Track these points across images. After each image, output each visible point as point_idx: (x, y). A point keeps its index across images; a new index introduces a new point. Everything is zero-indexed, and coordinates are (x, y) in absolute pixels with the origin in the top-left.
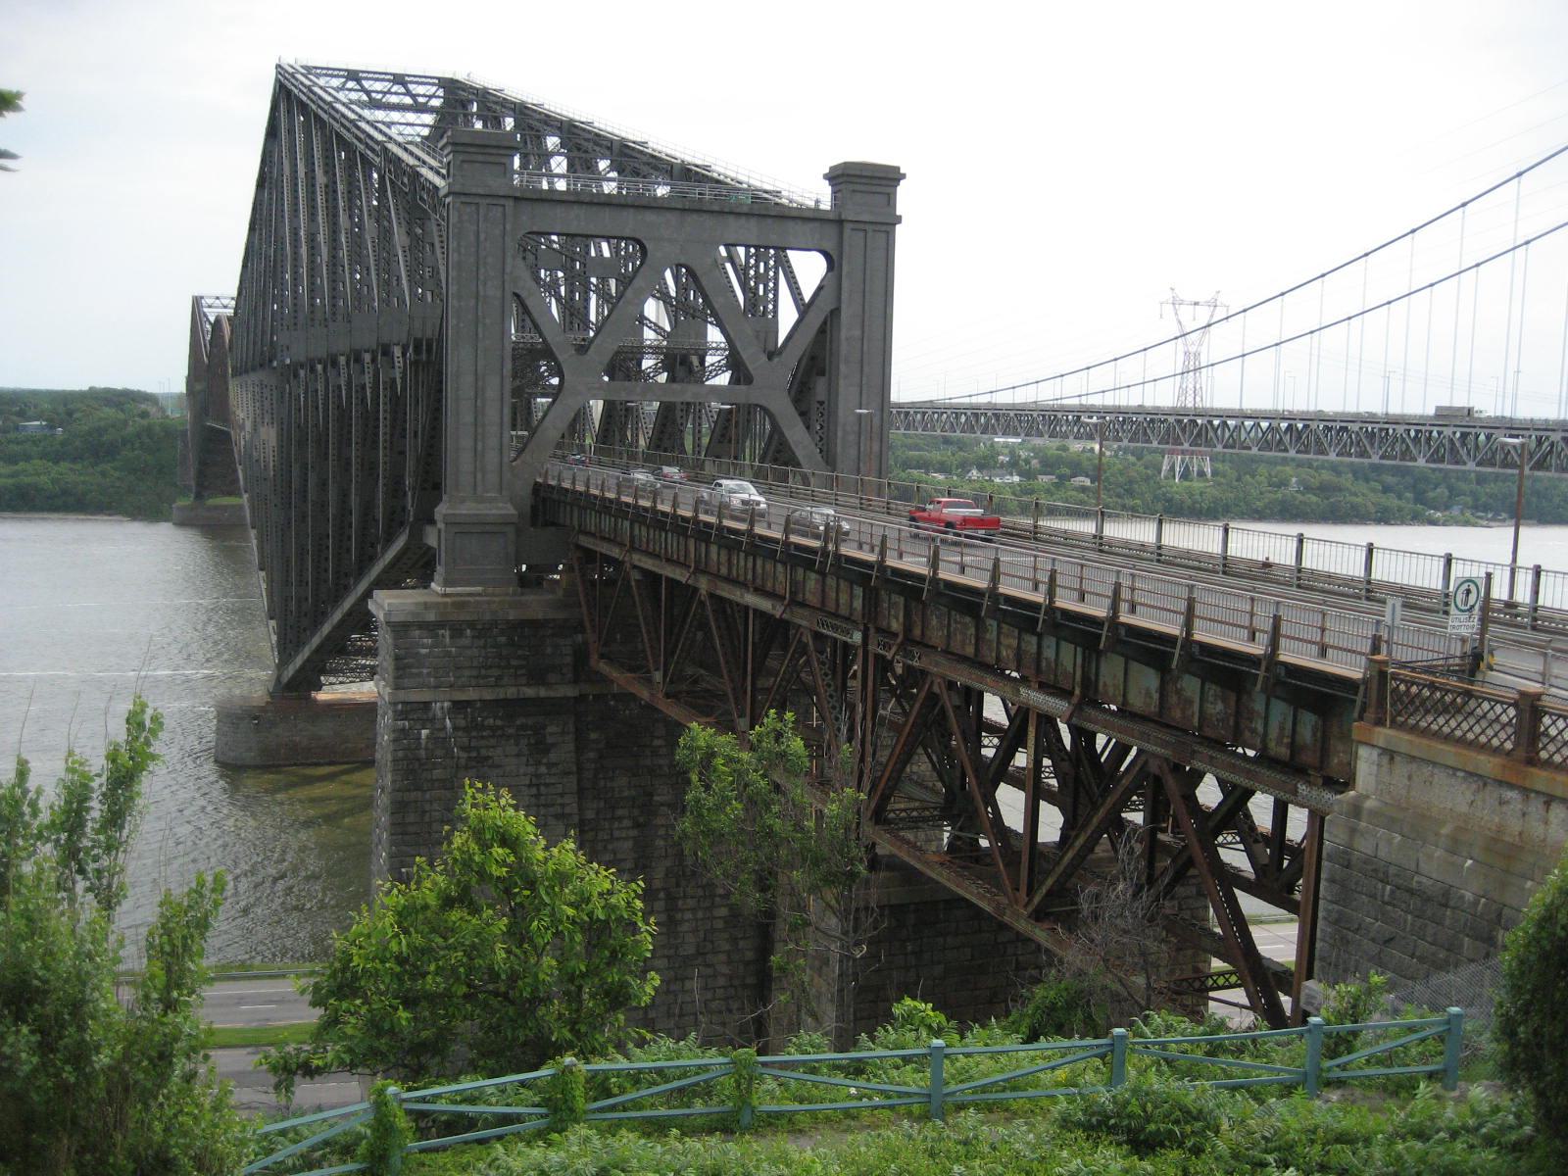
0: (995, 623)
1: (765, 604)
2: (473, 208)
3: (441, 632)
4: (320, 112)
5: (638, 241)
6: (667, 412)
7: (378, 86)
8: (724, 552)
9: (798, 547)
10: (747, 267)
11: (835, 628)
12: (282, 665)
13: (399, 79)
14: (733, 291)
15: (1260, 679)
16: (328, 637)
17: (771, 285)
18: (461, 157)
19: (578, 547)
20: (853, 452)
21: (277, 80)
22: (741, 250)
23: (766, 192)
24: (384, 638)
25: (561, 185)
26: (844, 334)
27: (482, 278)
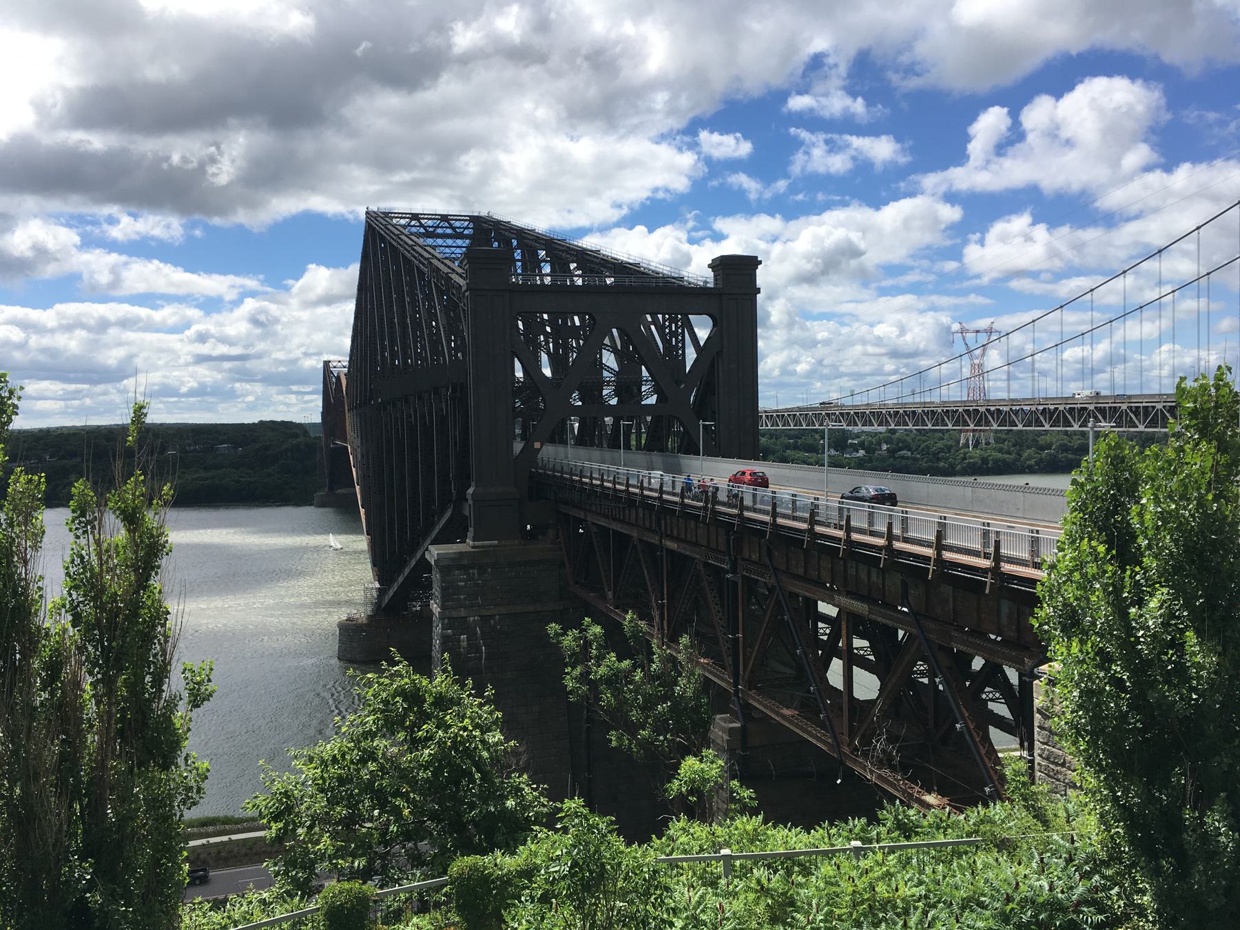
0: (816, 553)
4: (392, 241)
8: (647, 512)
10: (683, 326)
14: (655, 340)
15: (931, 571)
17: (680, 338)
22: (660, 316)
23: (674, 278)
24: (436, 576)
25: (548, 280)
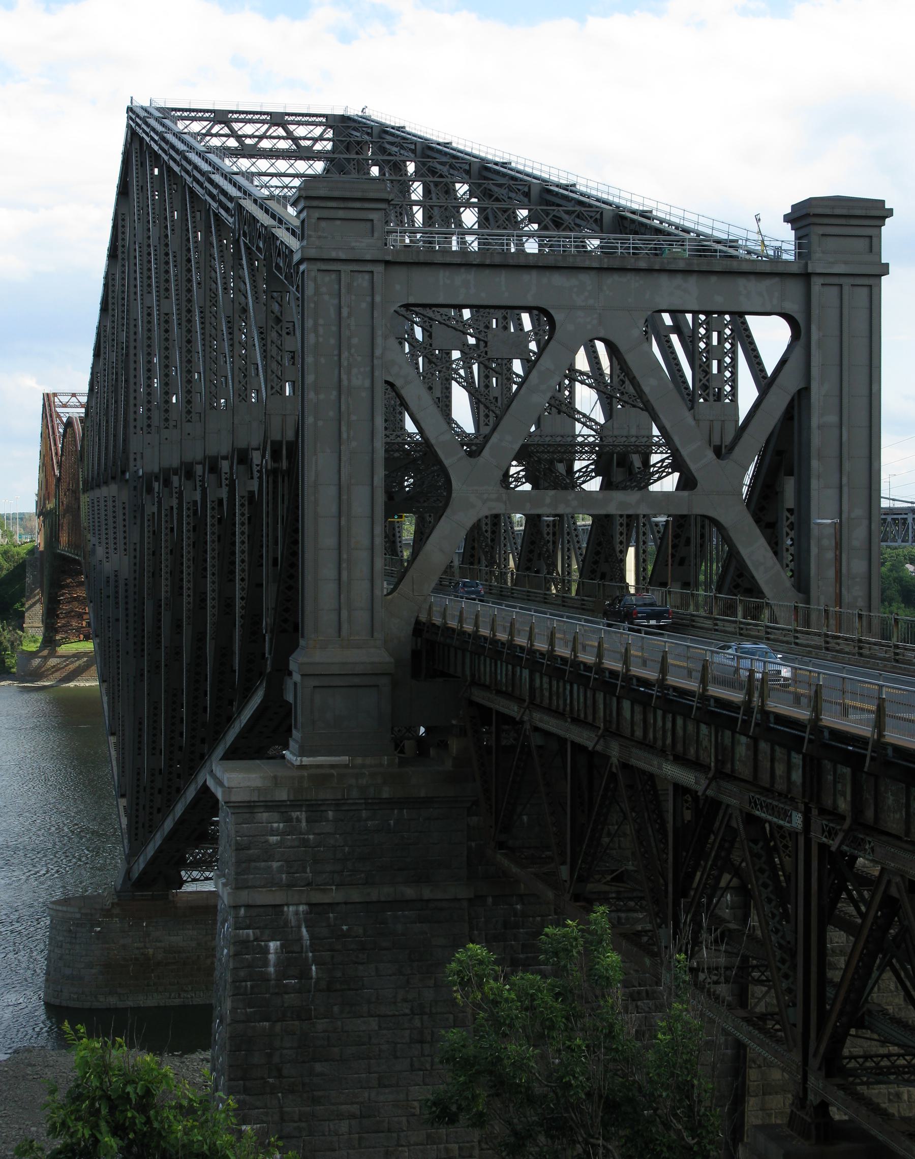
1: (687, 777)
2: (334, 276)
3: (295, 815)
4: (172, 164)
5: (543, 311)
6: (602, 523)
7: (249, 129)
8: (638, 709)
9: (719, 701)
11: (772, 810)
12: (132, 855)
13: (278, 119)
16: (181, 822)
18: (317, 214)
19: (471, 703)
20: (831, 573)
21: (129, 126)
26: (815, 422)
27: (345, 363)
